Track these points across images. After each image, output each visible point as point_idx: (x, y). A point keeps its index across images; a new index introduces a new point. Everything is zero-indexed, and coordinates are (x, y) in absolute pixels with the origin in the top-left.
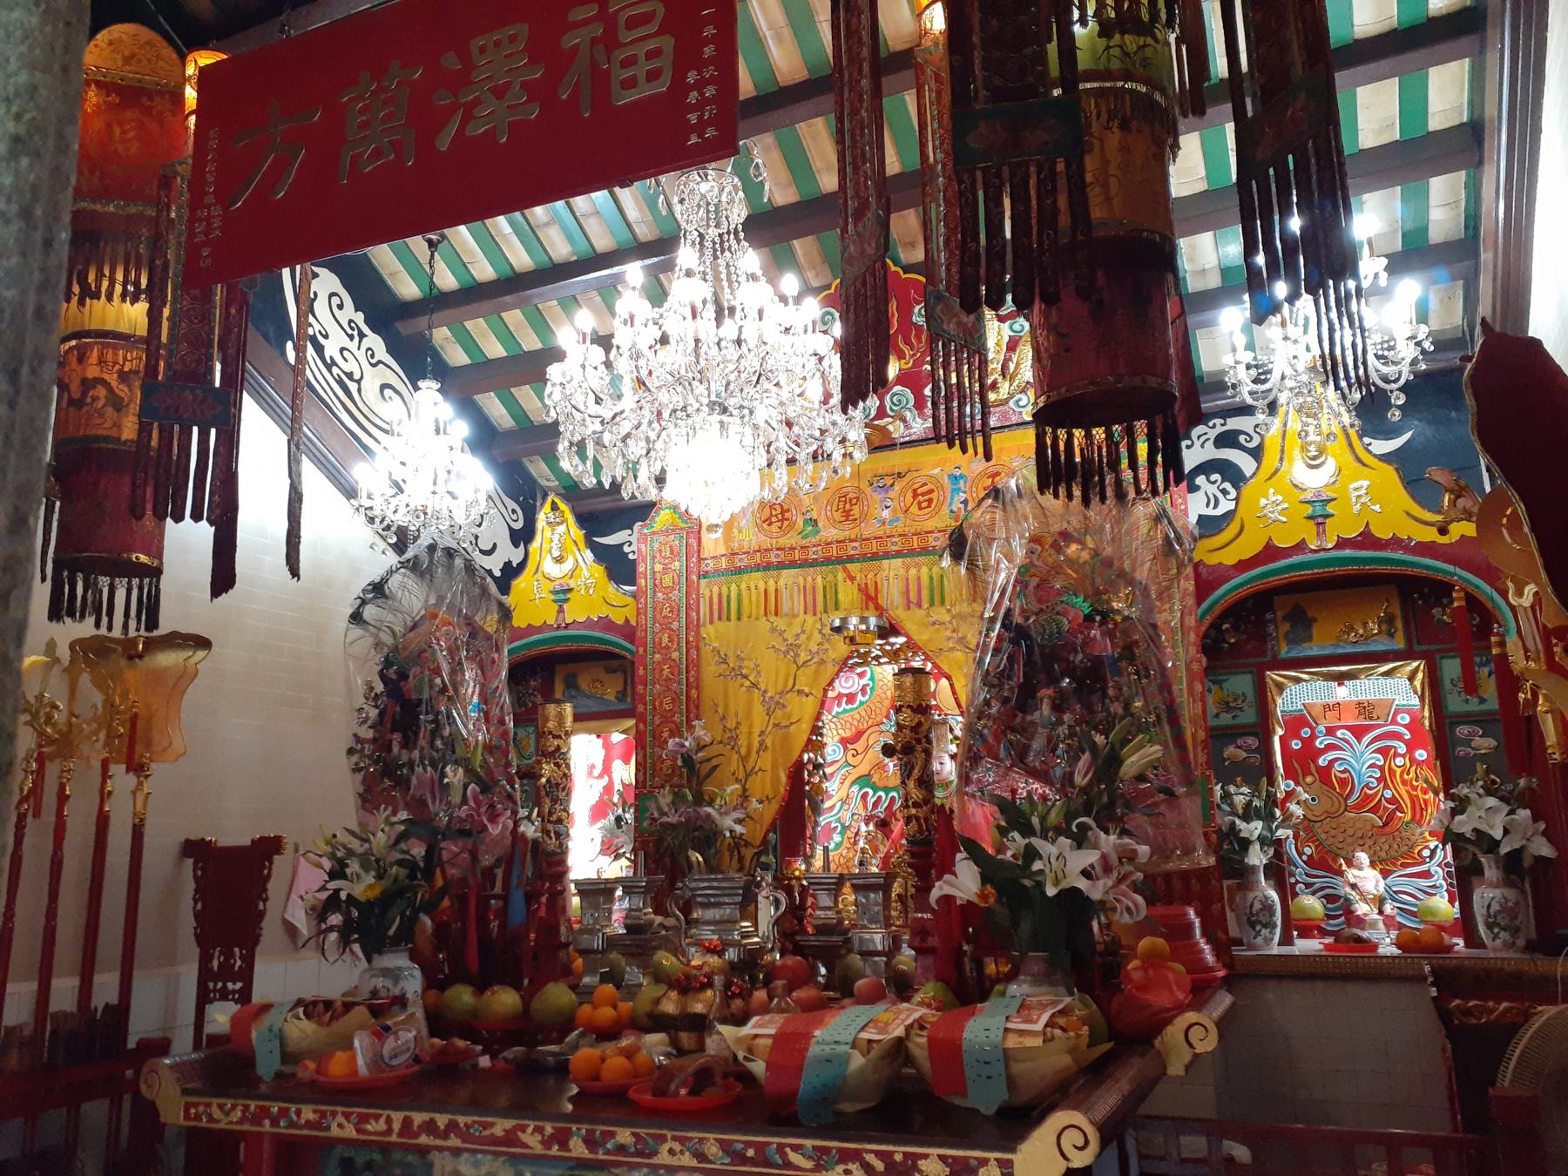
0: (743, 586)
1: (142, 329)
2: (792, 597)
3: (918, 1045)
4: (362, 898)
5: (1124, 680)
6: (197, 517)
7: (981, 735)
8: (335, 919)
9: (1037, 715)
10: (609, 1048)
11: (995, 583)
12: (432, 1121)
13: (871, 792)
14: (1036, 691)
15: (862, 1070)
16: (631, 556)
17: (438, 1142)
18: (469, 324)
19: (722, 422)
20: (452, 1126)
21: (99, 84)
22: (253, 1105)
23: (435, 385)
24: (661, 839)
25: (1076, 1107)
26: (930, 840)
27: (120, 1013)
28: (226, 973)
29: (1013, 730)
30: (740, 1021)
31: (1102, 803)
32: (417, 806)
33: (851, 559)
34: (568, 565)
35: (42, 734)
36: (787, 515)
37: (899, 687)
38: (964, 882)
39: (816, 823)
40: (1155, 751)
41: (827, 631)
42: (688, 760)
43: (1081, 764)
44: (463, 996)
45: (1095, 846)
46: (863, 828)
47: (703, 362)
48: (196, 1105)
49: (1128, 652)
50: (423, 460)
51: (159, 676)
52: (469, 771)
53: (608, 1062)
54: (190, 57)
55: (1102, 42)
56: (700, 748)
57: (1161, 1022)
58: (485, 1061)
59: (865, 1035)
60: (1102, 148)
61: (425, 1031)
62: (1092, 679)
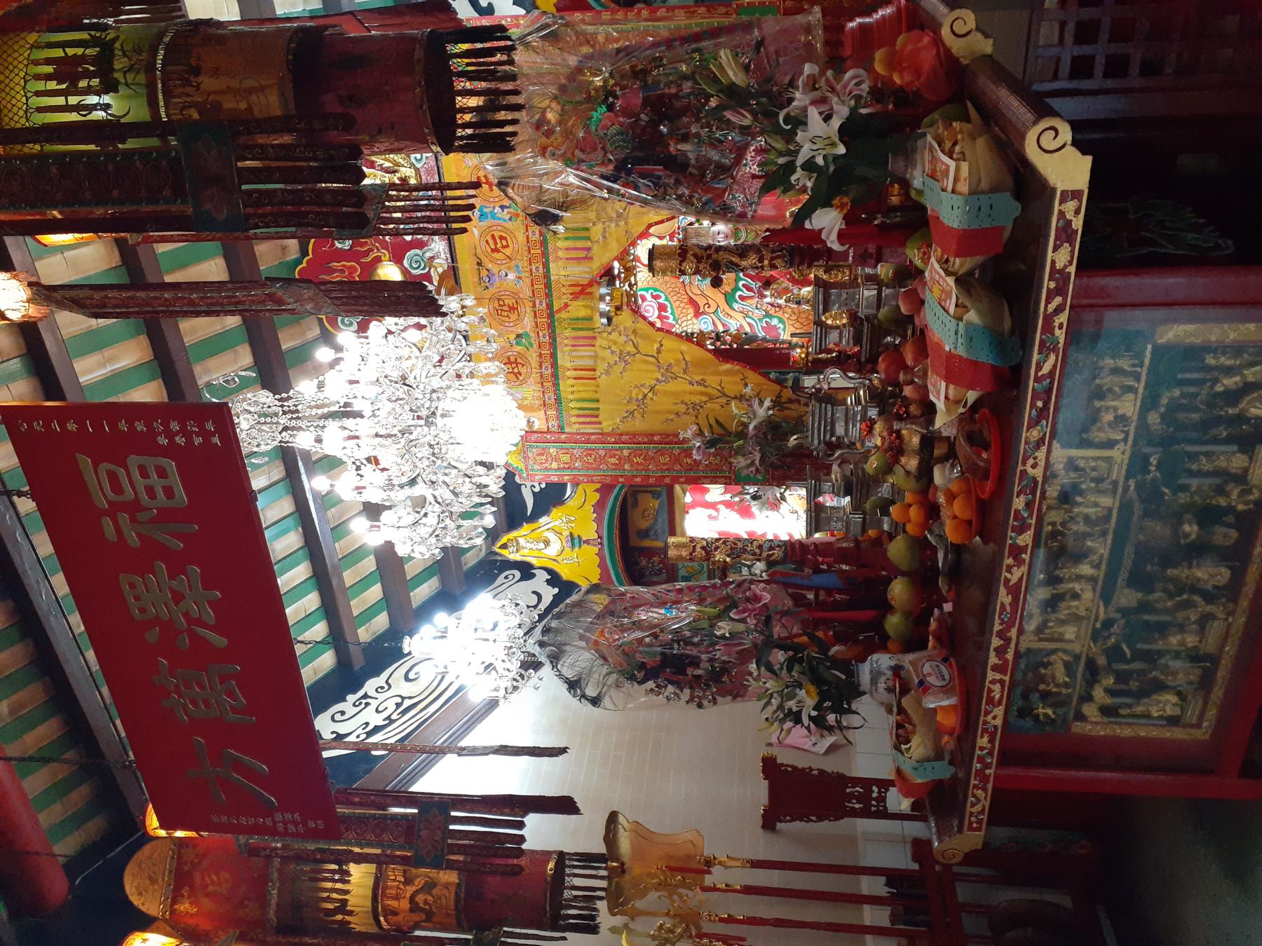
0: (571, 397)
1: (372, 868)
2: (582, 357)
3: (961, 265)
4: (817, 700)
5: (663, 79)
6: (521, 825)
7: (705, 204)
8: (831, 718)
9: (691, 155)
10: (945, 513)
11: (578, 187)
12: (995, 650)
13: (739, 293)
14: (671, 156)
15: (979, 313)
16: (543, 486)
17: (1013, 645)
18: (355, 613)
19: (443, 416)
20: (1001, 635)
21: (174, 902)
22: (973, 782)
23: (407, 640)
24: (772, 465)
25: (1023, 137)
26: (793, 249)
27: (892, 876)
28: (865, 798)
29: (703, 176)
30: (930, 410)
31: (767, 102)
32: (744, 657)
33: (550, 306)
34: (551, 536)
35: (681, 936)
36: (512, 359)
37: (664, 272)
38: (828, 221)
39: (764, 339)
40: (725, 55)
41: (609, 329)
42: (711, 443)
43: (733, 119)
44: (893, 622)
45: (805, 110)
46: (768, 300)
47: (395, 431)
48: (971, 823)
49: (639, 74)
50: (467, 648)
51: (637, 851)
52: (719, 617)
53: (958, 514)
54: (152, 833)
55: (123, 90)
56: (700, 433)
57: (949, 61)
58: (948, 607)
59: (952, 309)
60: (216, 92)
61: (924, 653)
62: (662, 107)
